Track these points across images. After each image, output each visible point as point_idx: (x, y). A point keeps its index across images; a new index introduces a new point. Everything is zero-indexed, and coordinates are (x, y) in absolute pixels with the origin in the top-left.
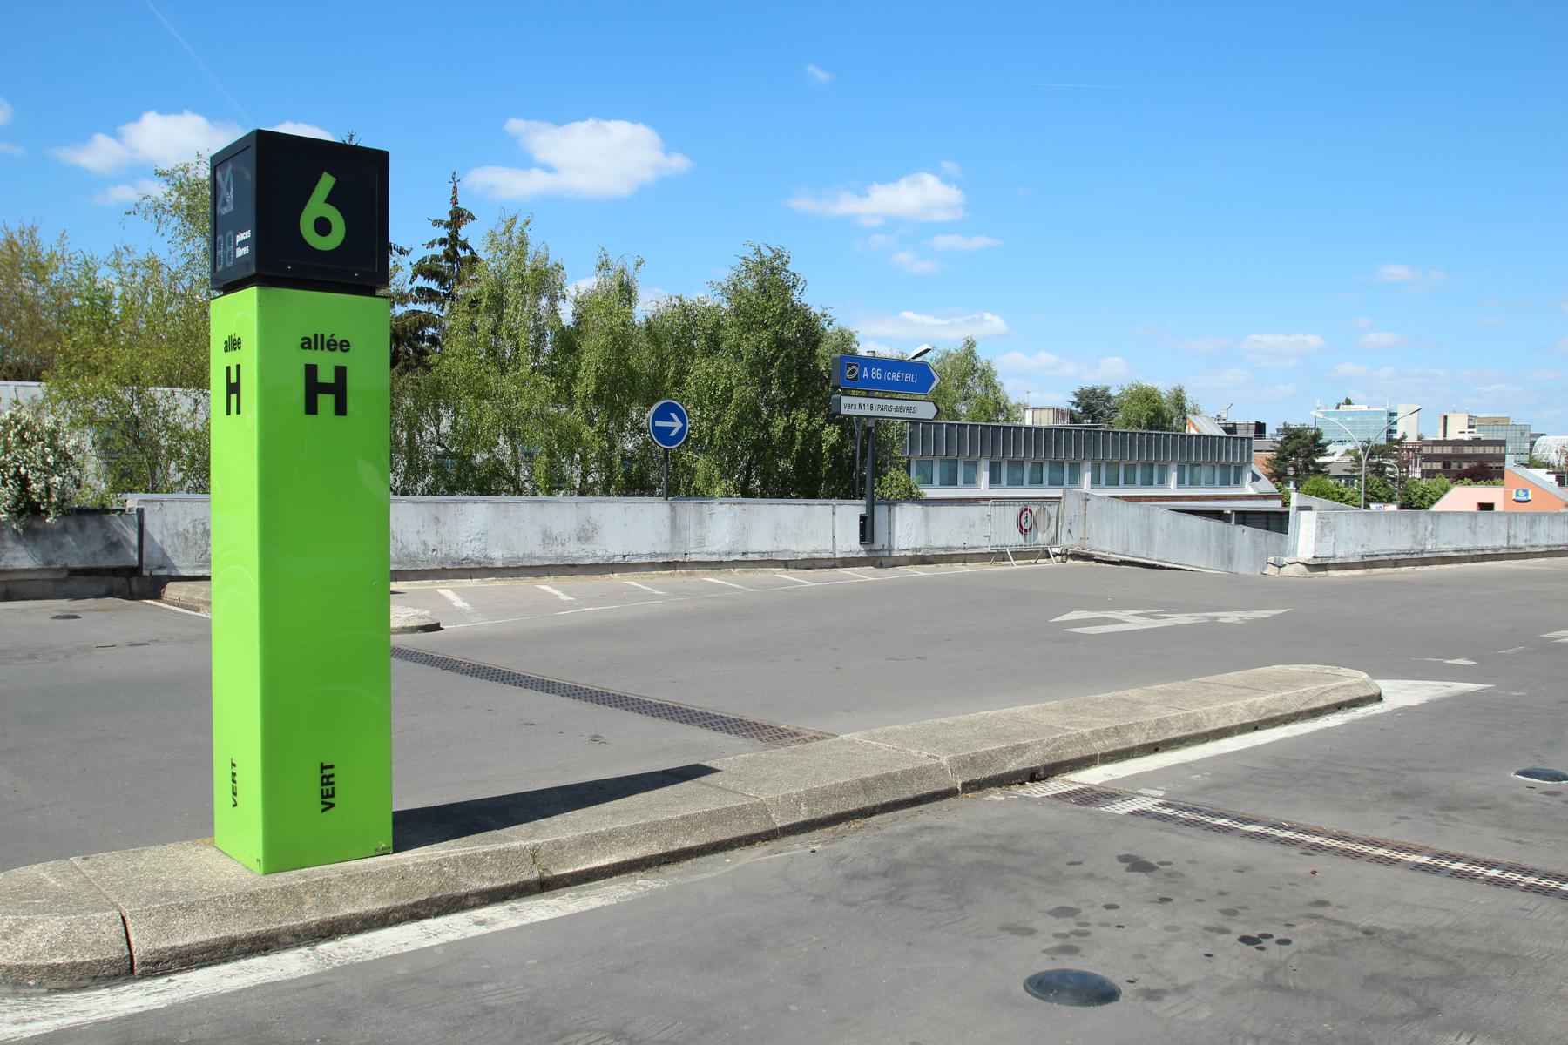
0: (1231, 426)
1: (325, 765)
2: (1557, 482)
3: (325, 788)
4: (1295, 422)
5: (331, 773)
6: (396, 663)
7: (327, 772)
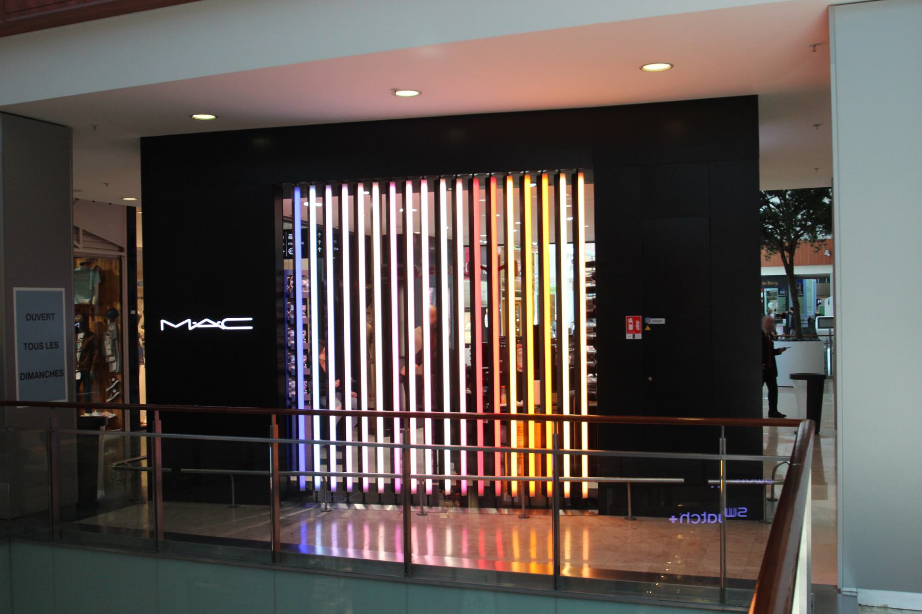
7: (51, 316)
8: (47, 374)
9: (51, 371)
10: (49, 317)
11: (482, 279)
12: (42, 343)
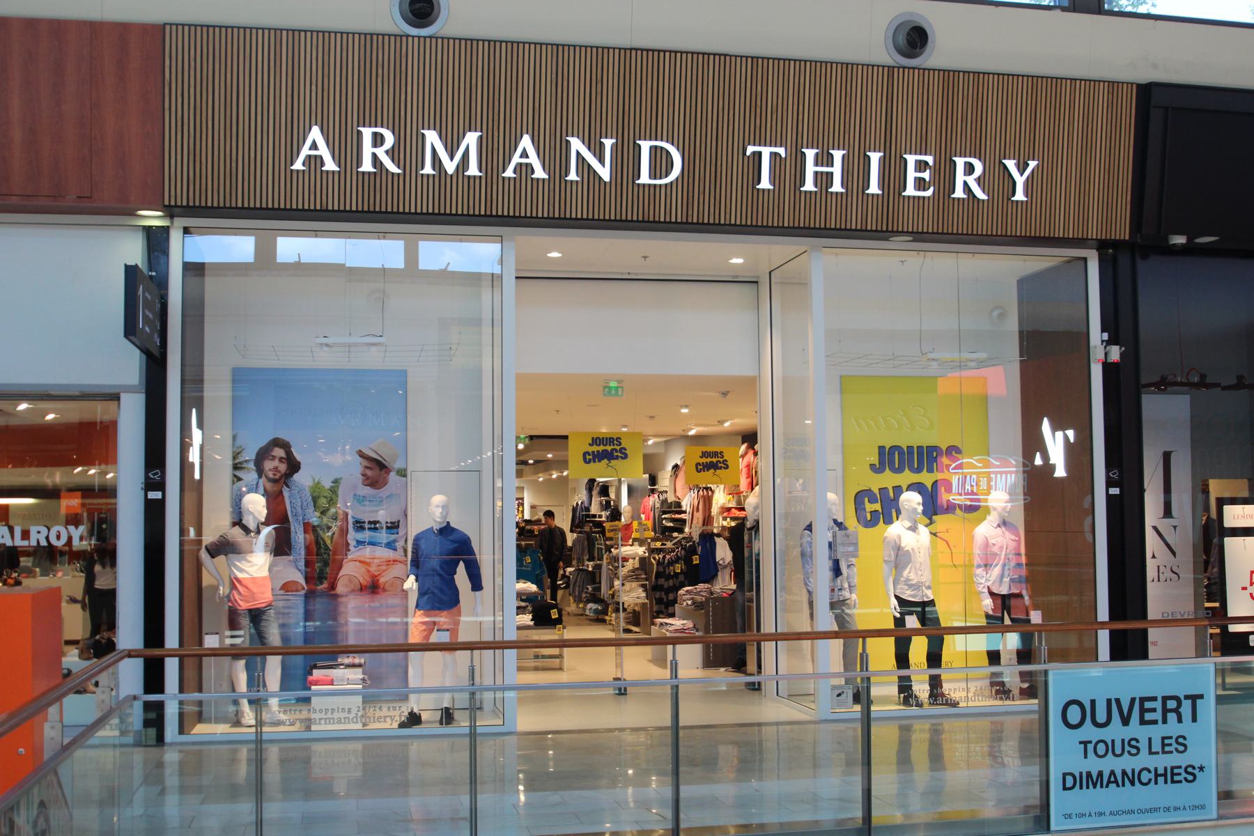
0: (598, 581)
1: (1199, 701)
2: (988, 517)
3: (1158, 705)
4: (893, 525)
5: (1154, 707)
6: (779, 673)
7: (1186, 707)
8: (1145, 777)
9: (1156, 769)
10: (1176, 711)
11: (498, 477)
12: (1137, 741)
